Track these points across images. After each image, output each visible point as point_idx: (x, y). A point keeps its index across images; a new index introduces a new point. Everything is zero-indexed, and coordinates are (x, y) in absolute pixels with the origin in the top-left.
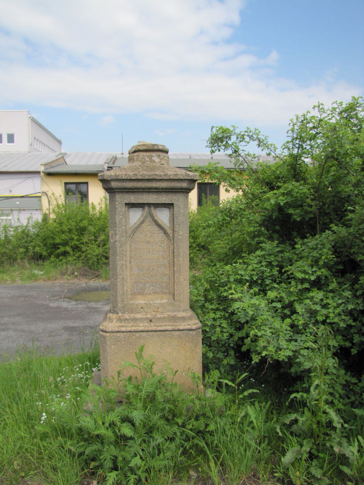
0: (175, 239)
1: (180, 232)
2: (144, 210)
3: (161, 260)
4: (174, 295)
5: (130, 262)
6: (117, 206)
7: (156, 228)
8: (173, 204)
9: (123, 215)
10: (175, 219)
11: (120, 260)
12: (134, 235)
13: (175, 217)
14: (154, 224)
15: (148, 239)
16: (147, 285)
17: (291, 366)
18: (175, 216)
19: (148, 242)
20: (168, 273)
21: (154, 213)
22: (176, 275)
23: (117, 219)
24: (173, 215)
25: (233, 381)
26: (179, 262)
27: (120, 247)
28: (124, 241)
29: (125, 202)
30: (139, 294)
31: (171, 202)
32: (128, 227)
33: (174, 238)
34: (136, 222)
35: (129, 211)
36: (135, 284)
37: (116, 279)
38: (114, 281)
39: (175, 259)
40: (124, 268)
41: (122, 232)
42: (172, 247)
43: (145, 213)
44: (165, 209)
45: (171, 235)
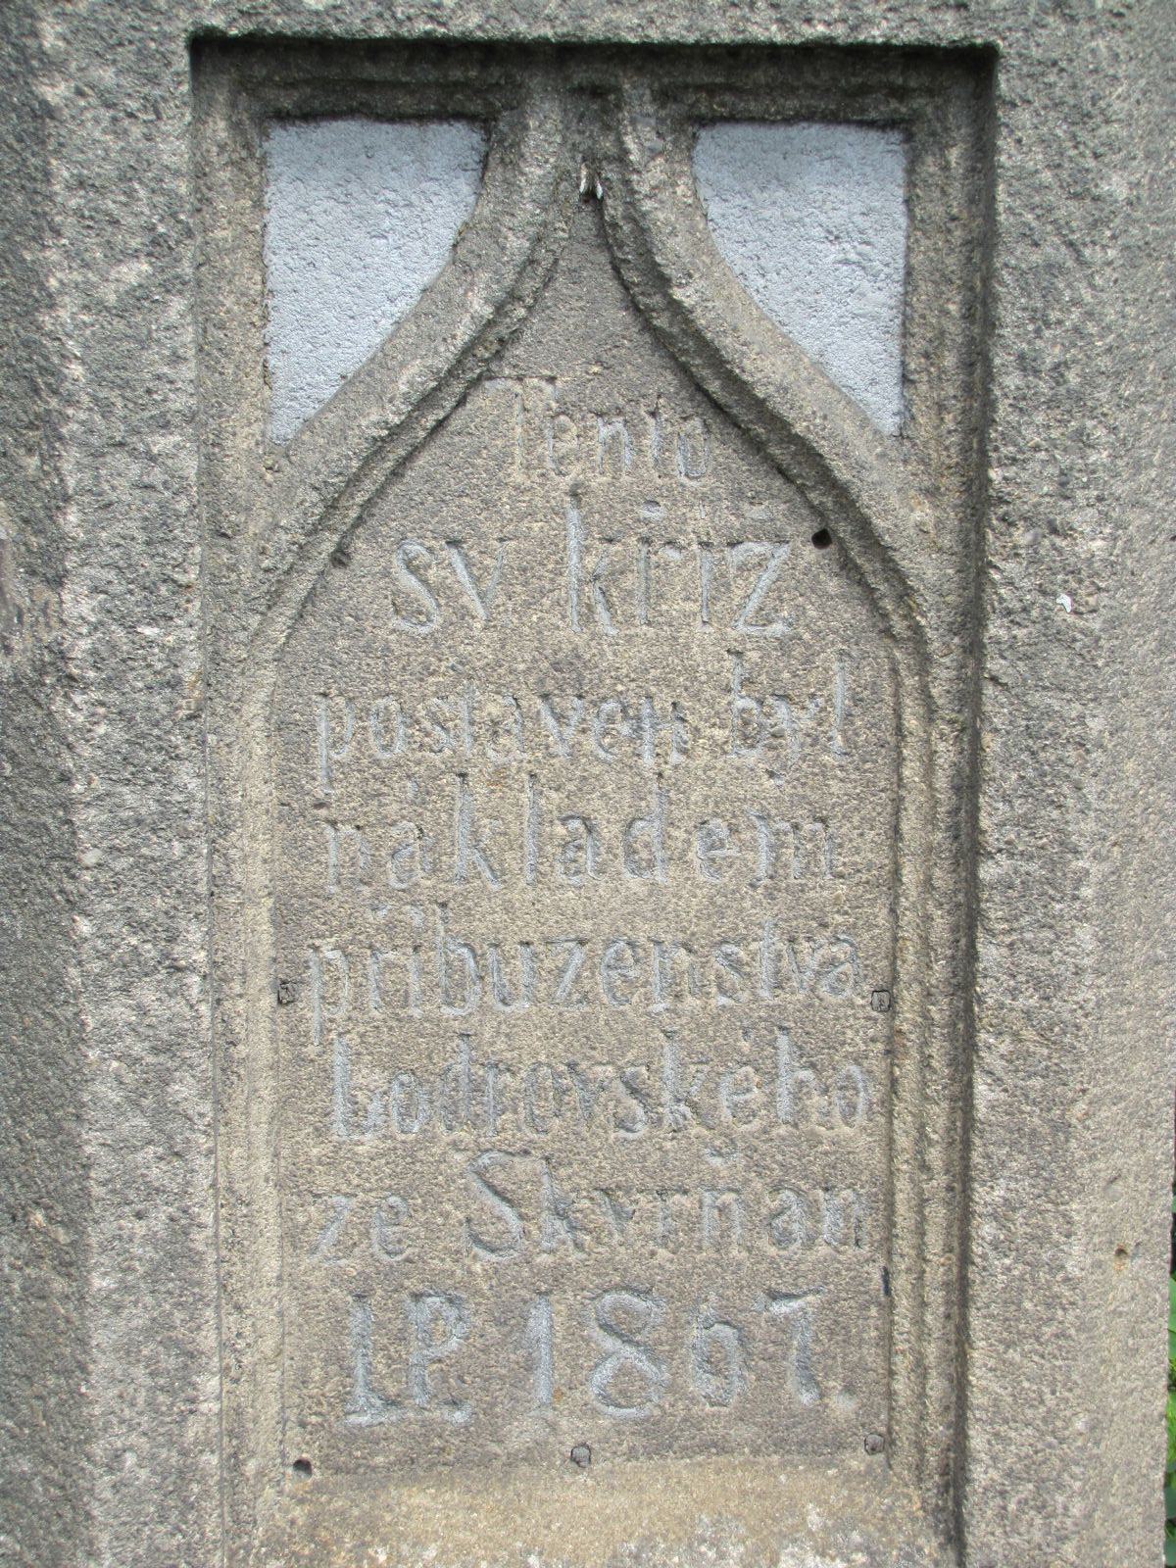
0: (996, 629)
1: (1082, 519)
2: (497, 154)
3: (767, 945)
4: (955, 1476)
5: (286, 992)
6: (55, 92)
7: (684, 465)
8: (975, 65)
9: (157, 246)
10: (1010, 314)
11: (131, 969)
12: (340, 558)
13: (1007, 287)
14: (668, 381)
15: (569, 634)
16: (540, 1321)
18: (1013, 256)
19: (566, 677)
20: (857, 1136)
21: (660, 214)
22: (987, 1196)
23: (67, 312)
24: (984, 242)
26: (1047, 986)
27: (125, 766)
28: (192, 665)
29: (184, 23)
30: (426, 1459)
31: (948, 28)
32: (242, 441)
33: (971, 619)
34: (381, 362)
35: (251, 163)
36: (356, 1321)
37: (70, 1263)
38: (37, 1292)
39: (990, 953)
40: (183, 1089)
41: (159, 530)
42: (946, 753)
43: (528, 210)
44: (849, 141)
45: (930, 570)
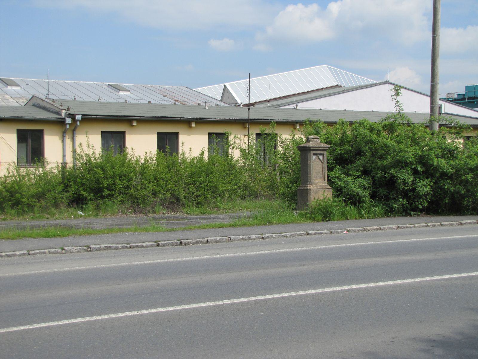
17: (47, 176)
25: (346, 198)
45: (323, 163)
